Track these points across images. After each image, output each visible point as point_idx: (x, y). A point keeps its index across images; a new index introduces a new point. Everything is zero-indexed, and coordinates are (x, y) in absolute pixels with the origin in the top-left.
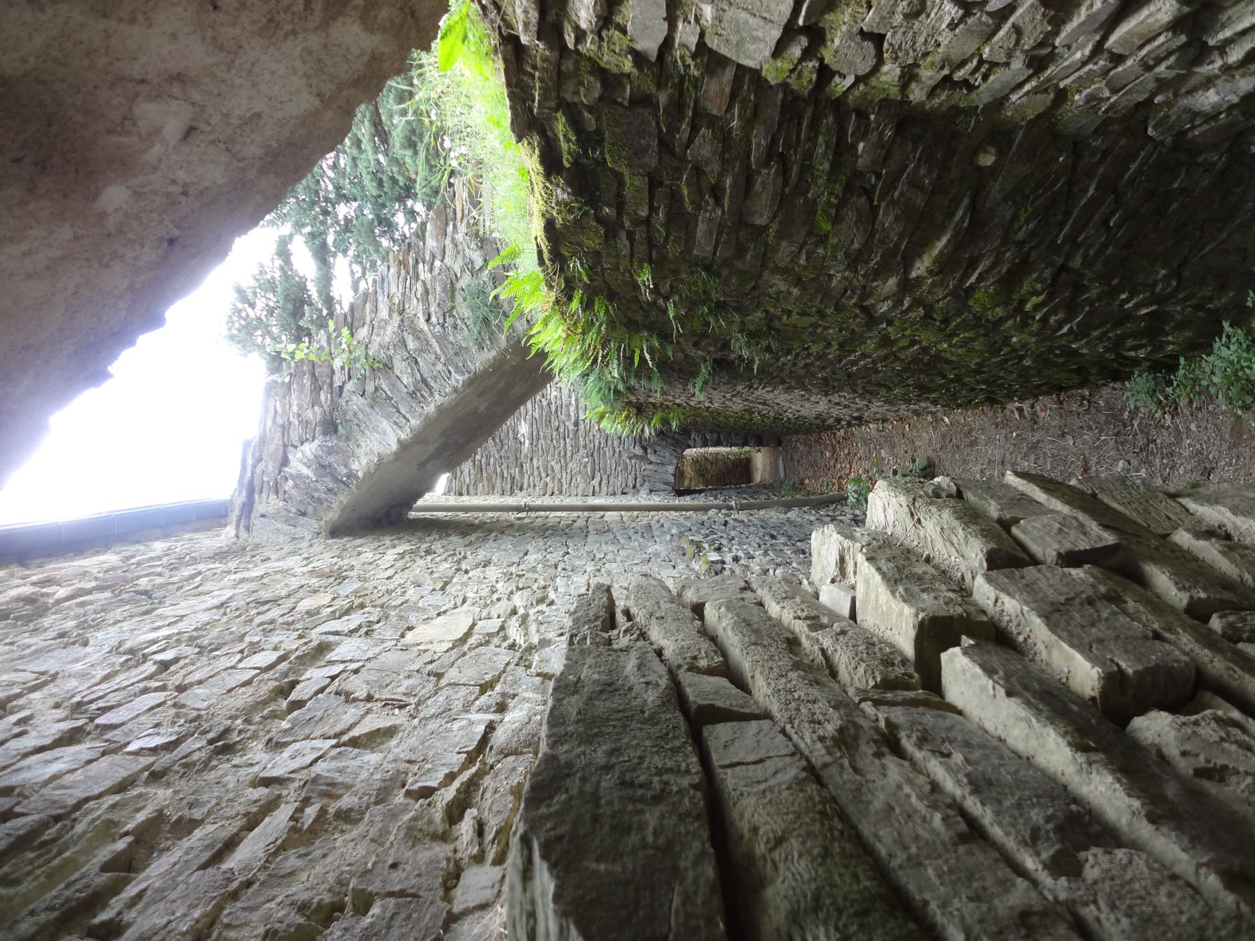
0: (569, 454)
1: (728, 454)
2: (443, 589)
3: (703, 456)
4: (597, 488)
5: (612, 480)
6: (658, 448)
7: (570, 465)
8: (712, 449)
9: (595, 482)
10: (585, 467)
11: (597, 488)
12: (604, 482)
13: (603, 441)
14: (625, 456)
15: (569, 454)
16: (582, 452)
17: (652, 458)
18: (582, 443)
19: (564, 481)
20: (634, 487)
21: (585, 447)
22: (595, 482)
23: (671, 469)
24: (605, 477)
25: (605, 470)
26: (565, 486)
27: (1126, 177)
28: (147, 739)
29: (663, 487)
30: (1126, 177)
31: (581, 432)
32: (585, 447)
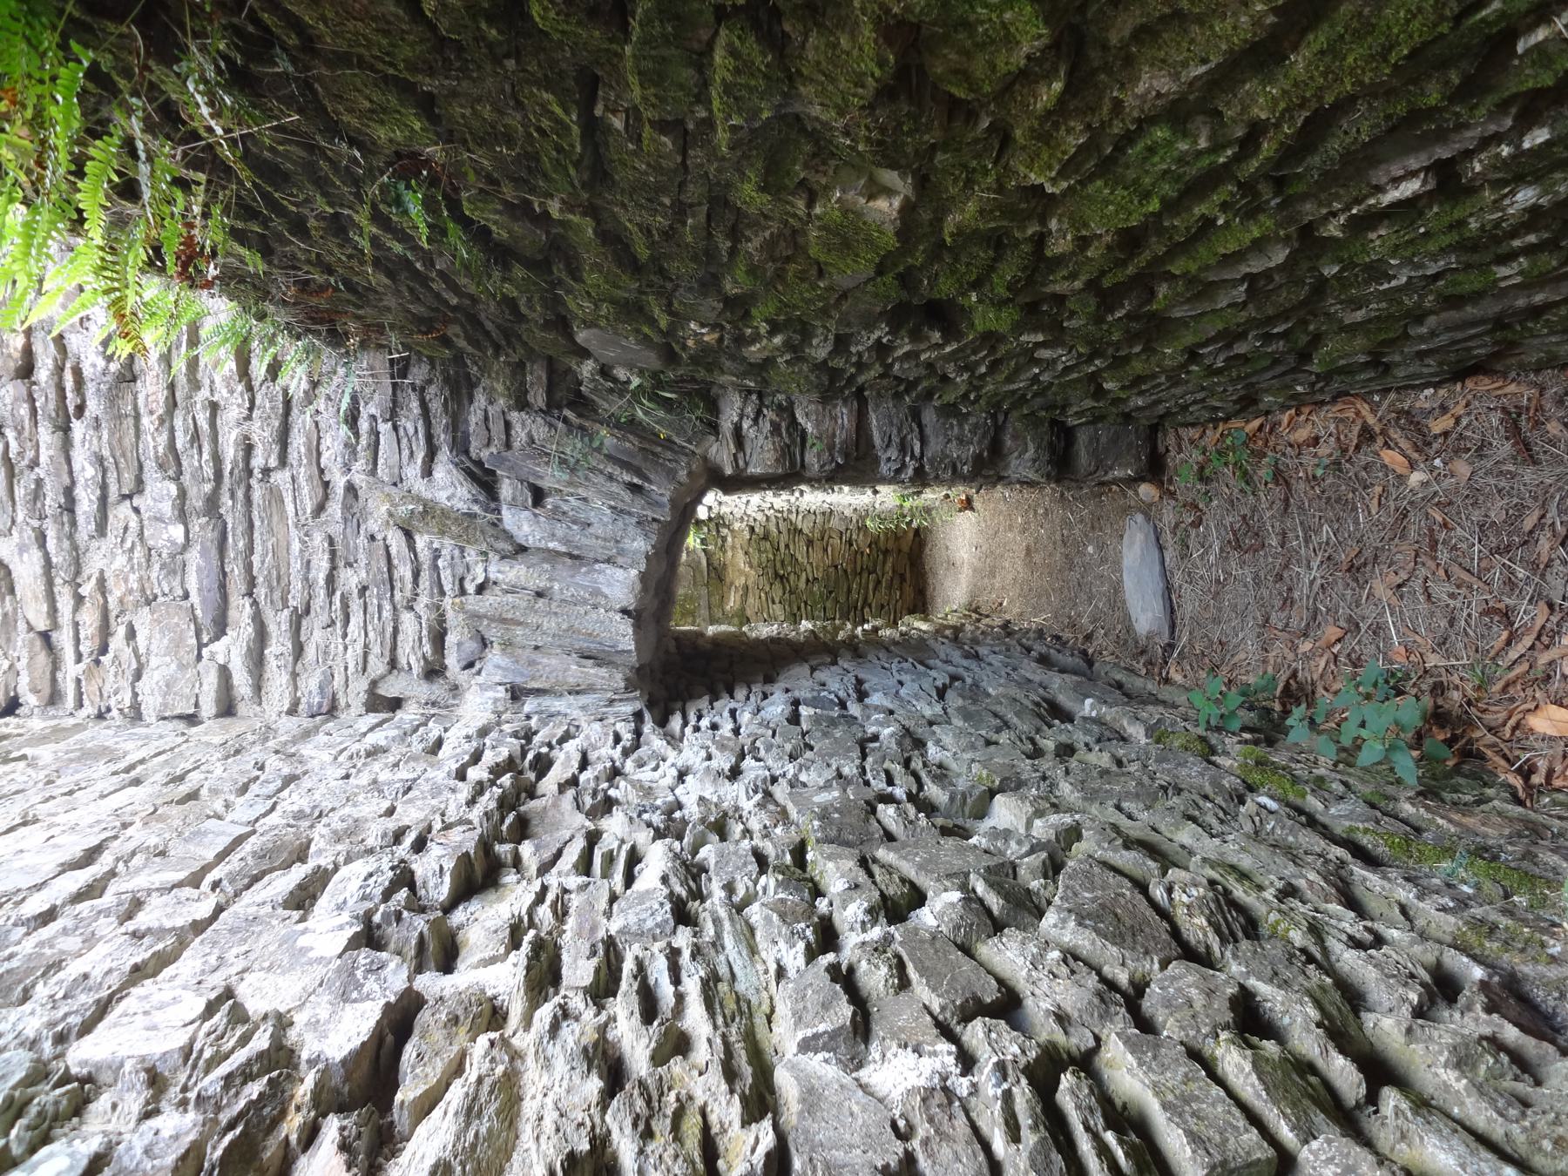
0: (86, 502)
1: (863, 515)
2: (39, 293)
3: (783, 518)
4: (241, 681)
5: (315, 635)
6: (551, 477)
7: (95, 563)
8: (812, 499)
9: (232, 648)
10: (176, 567)
11: (241, 681)
12: (278, 645)
13: (262, 433)
14: (378, 511)
15: (86, 502)
16: (159, 493)
17: (520, 523)
18: (154, 443)
19: (64, 639)
20: (434, 672)
21: (172, 462)
22: (232, 648)
23: (620, 584)
24: (278, 625)
25: (280, 582)
26: (71, 670)
27: (1478, 17)
28: (1154, 584)
29: (576, 672)
30: (1478, 17)
31: (150, 390)
32: (172, 462)
